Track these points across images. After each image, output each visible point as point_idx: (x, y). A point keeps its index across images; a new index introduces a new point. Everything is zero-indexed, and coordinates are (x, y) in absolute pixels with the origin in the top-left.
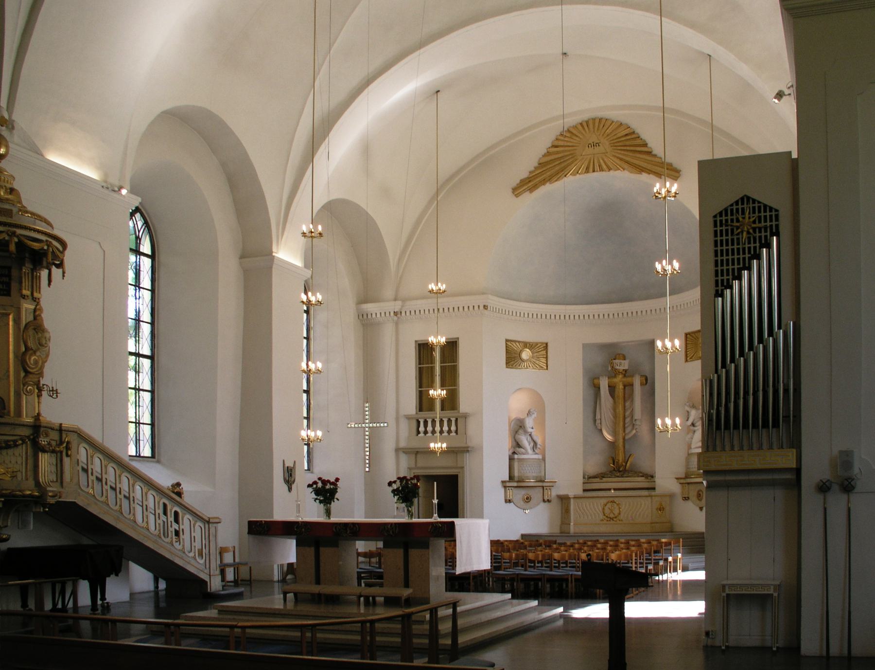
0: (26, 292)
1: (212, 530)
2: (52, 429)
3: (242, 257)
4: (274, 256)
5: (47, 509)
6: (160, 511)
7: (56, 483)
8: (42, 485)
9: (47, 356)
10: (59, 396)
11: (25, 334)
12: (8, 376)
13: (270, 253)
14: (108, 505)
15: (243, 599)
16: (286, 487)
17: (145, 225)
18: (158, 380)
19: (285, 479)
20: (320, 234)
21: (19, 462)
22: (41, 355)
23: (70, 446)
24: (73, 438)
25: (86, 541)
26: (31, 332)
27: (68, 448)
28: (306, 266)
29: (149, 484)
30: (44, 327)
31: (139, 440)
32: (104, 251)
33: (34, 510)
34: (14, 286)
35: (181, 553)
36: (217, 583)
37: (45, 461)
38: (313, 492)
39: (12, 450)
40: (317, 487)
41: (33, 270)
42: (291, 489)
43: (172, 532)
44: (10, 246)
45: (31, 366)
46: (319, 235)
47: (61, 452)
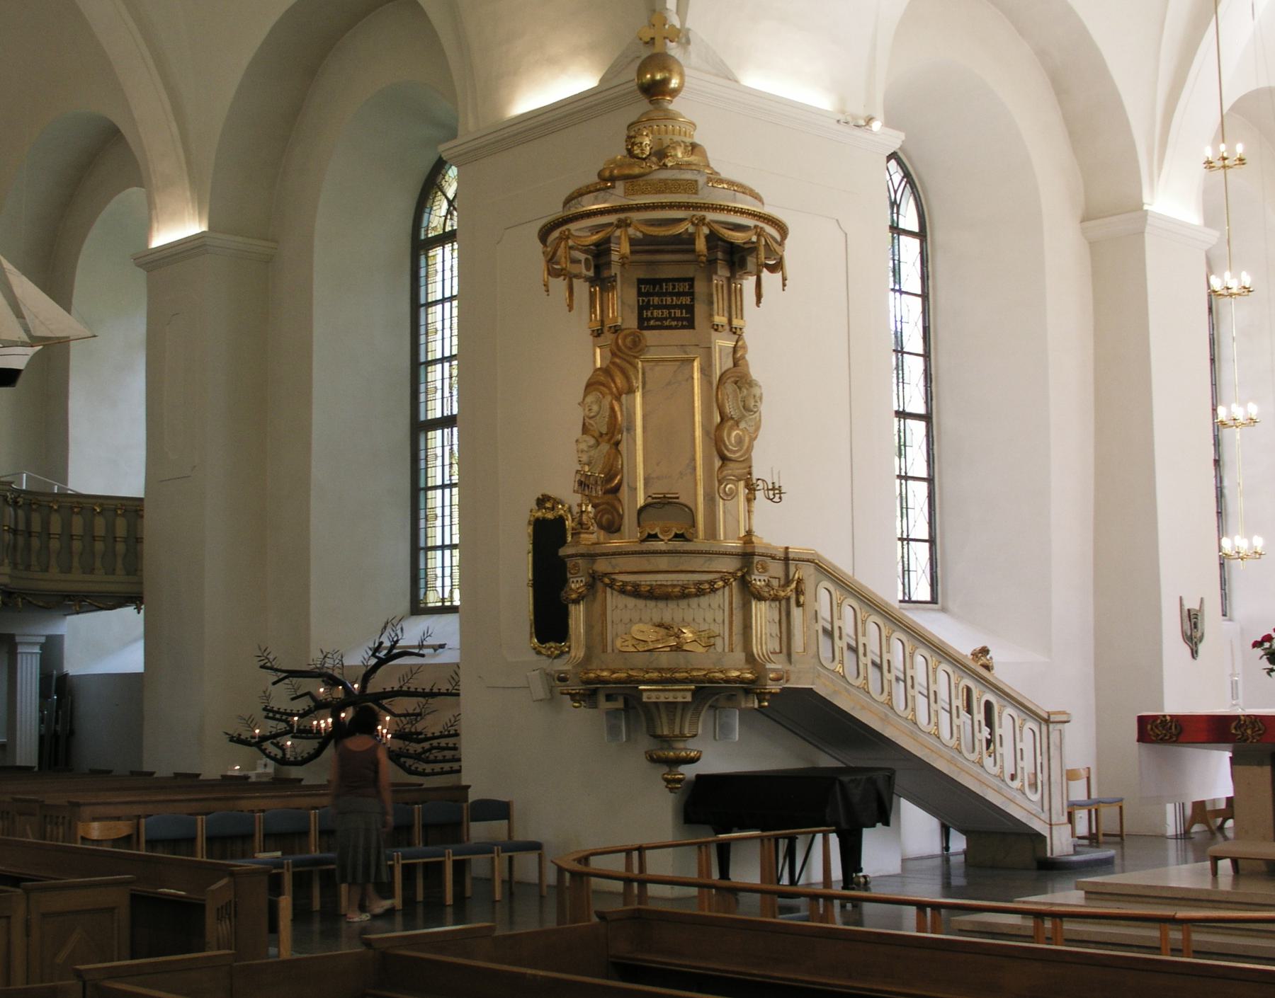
0: (720, 319)
1: (1054, 737)
2: (773, 558)
3: (1084, 219)
4: (1147, 211)
5: (766, 704)
6: (959, 702)
7: (780, 655)
8: (758, 661)
9: (758, 428)
10: (783, 499)
11: (719, 393)
12: (694, 469)
13: (1139, 206)
14: (868, 692)
15: (1113, 873)
16: (1186, 650)
17: (905, 180)
18: (939, 457)
19: (1184, 633)
20: (1241, 160)
21: (719, 619)
22: (748, 428)
23: (803, 588)
24: (807, 572)
25: (826, 761)
26: (729, 387)
27: (799, 592)
28: (1209, 221)
29: (940, 651)
30: (751, 377)
31: (909, 571)
32: (846, 234)
33: (743, 705)
34: (700, 310)
35: (997, 782)
36: (1064, 840)
37: (762, 613)
38: (1265, 657)
39: (707, 597)
40: (1271, 646)
41: (729, 279)
42: (1197, 652)
43: (980, 741)
44: (697, 242)
45: (730, 447)
46: (1237, 162)
47: (788, 599)
